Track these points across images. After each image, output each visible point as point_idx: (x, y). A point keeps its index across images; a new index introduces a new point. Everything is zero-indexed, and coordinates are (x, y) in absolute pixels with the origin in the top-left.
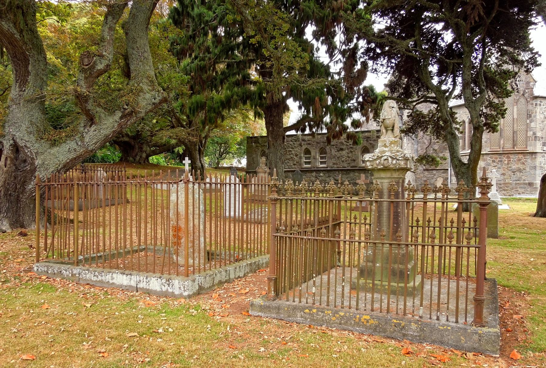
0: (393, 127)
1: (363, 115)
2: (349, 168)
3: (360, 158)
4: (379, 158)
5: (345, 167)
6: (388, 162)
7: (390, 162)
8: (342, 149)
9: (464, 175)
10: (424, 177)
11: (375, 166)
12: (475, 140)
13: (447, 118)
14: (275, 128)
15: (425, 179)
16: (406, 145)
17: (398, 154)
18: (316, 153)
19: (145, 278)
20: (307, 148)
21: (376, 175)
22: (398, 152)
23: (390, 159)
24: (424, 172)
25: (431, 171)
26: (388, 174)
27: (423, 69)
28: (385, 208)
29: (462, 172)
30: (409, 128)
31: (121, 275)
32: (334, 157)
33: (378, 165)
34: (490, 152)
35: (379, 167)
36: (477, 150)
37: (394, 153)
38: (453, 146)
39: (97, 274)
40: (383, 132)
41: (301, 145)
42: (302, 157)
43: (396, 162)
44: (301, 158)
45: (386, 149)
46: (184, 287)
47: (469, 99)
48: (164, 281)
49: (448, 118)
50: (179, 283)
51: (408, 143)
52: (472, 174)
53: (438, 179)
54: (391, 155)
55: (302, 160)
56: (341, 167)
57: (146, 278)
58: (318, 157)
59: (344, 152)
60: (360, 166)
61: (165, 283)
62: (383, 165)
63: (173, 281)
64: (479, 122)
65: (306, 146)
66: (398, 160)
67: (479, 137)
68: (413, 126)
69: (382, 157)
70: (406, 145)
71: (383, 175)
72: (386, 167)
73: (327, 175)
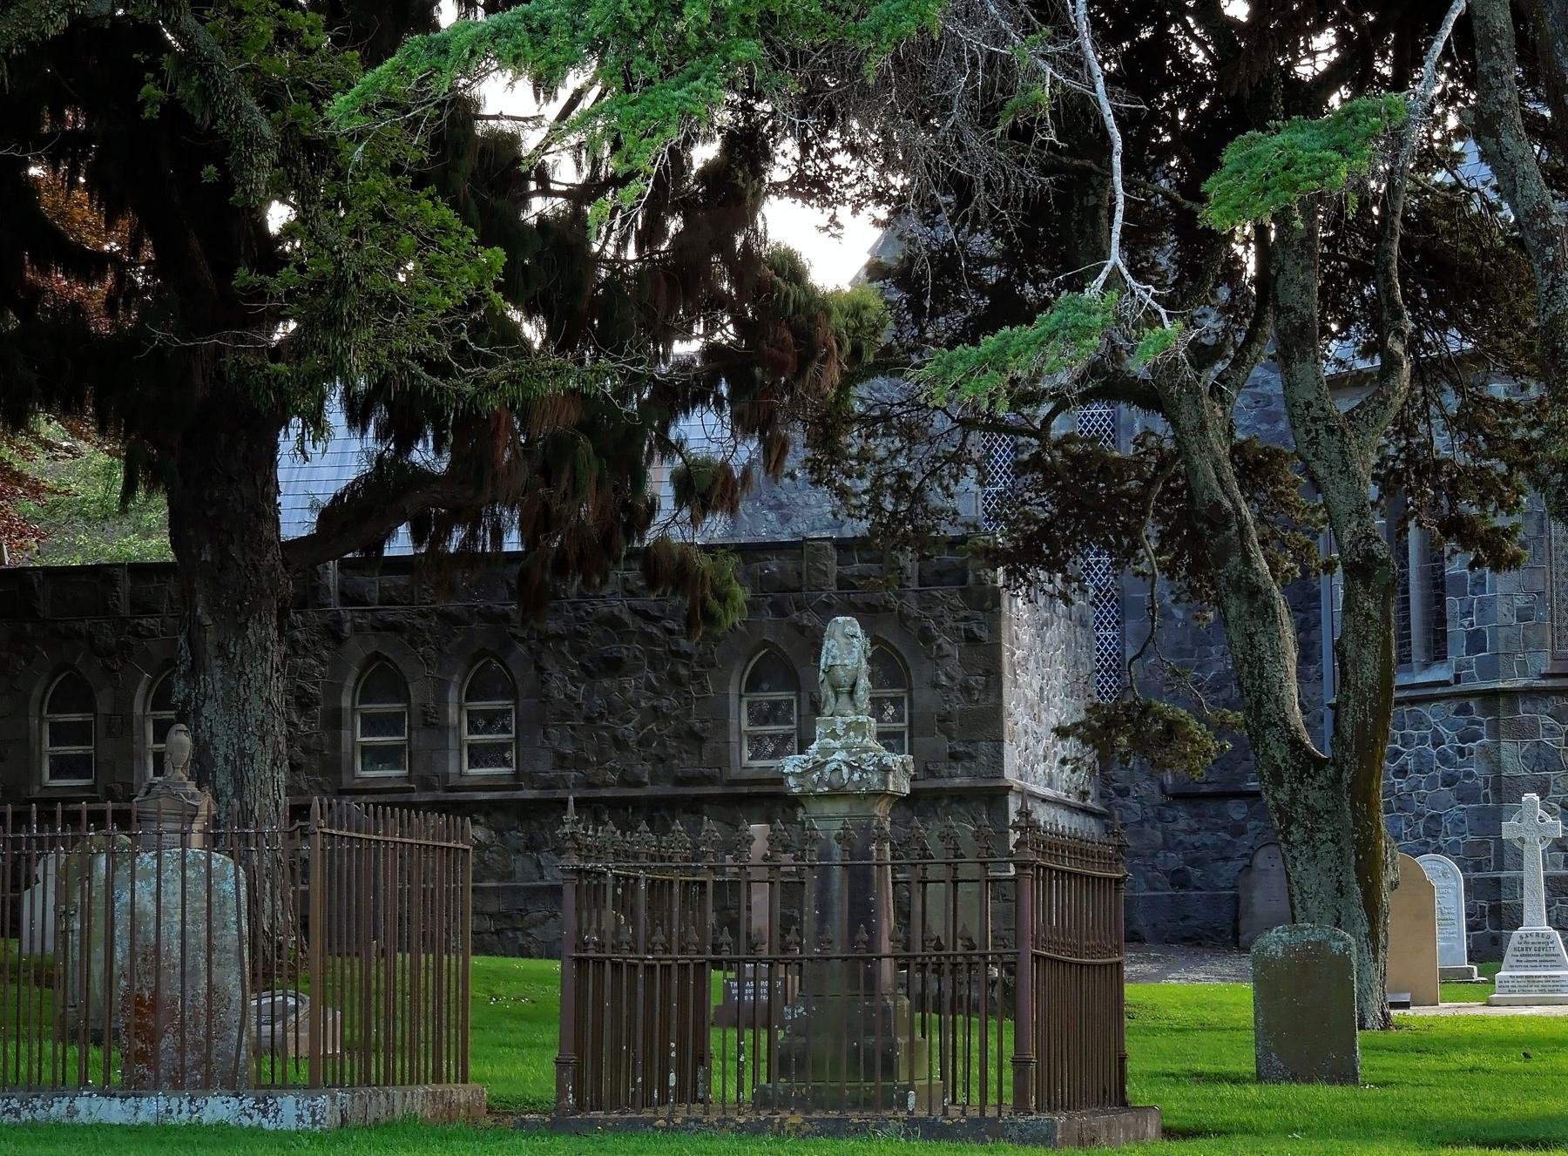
0: (854, 685)
1: (744, 424)
2: (665, 789)
3: (733, 721)
4: (819, 766)
5: (640, 784)
6: (841, 777)
7: (846, 776)
8: (614, 666)
9: (1322, 824)
10: (1166, 847)
11: (809, 786)
12: (1356, 631)
13: (1219, 504)
14: (234, 551)
15: (1175, 860)
16: (1025, 638)
17: (864, 756)
18: (441, 687)
19: (185, 1102)
20: (377, 656)
21: (815, 808)
22: (866, 752)
23: (845, 769)
24: (1169, 814)
25: (1210, 808)
26: (842, 808)
27: (1082, 233)
28: (836, 894)
29: (1307, 807)
30: (1029, 539)
31: (104, 1101)
32: (566, 716)
33: (816, 786)
34: (1543, 683)
35: (819, 790)
36: (1371, 688)
37: (855, 754)
38: (1261, 659)
39: (17, 1105)
40: (827, 697)
41: (333, 633)
42: (346, 717)
43: (861, 776)
44: (335, 720)
45: (837, 744)
46: (313, 1114)
47: (1315, 411)
48: (248, 1102)
49: (1227, 504)
50: (298, 1102)
51: (1047, 624)
52: (1356, 819)
53: (1261, 860)
54: (847, 759)
55: (345, 734)
56: (606, 785)
57: (190, 1102)
58: (452, 712)
59: (630, 683)
60: (734, 773)
61: (253, 1108)
62: (829, 784)
63: (279, 1100)
64: (1368, 537)
65: (374, 645)
66: (864, 771)
67: (1377, 615)
68: (1049, 524)
69: (826, 763)
70: (1025, 638)
71: (828, 808)
72: (837, 790)
73: (517, 837)
